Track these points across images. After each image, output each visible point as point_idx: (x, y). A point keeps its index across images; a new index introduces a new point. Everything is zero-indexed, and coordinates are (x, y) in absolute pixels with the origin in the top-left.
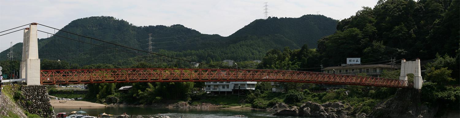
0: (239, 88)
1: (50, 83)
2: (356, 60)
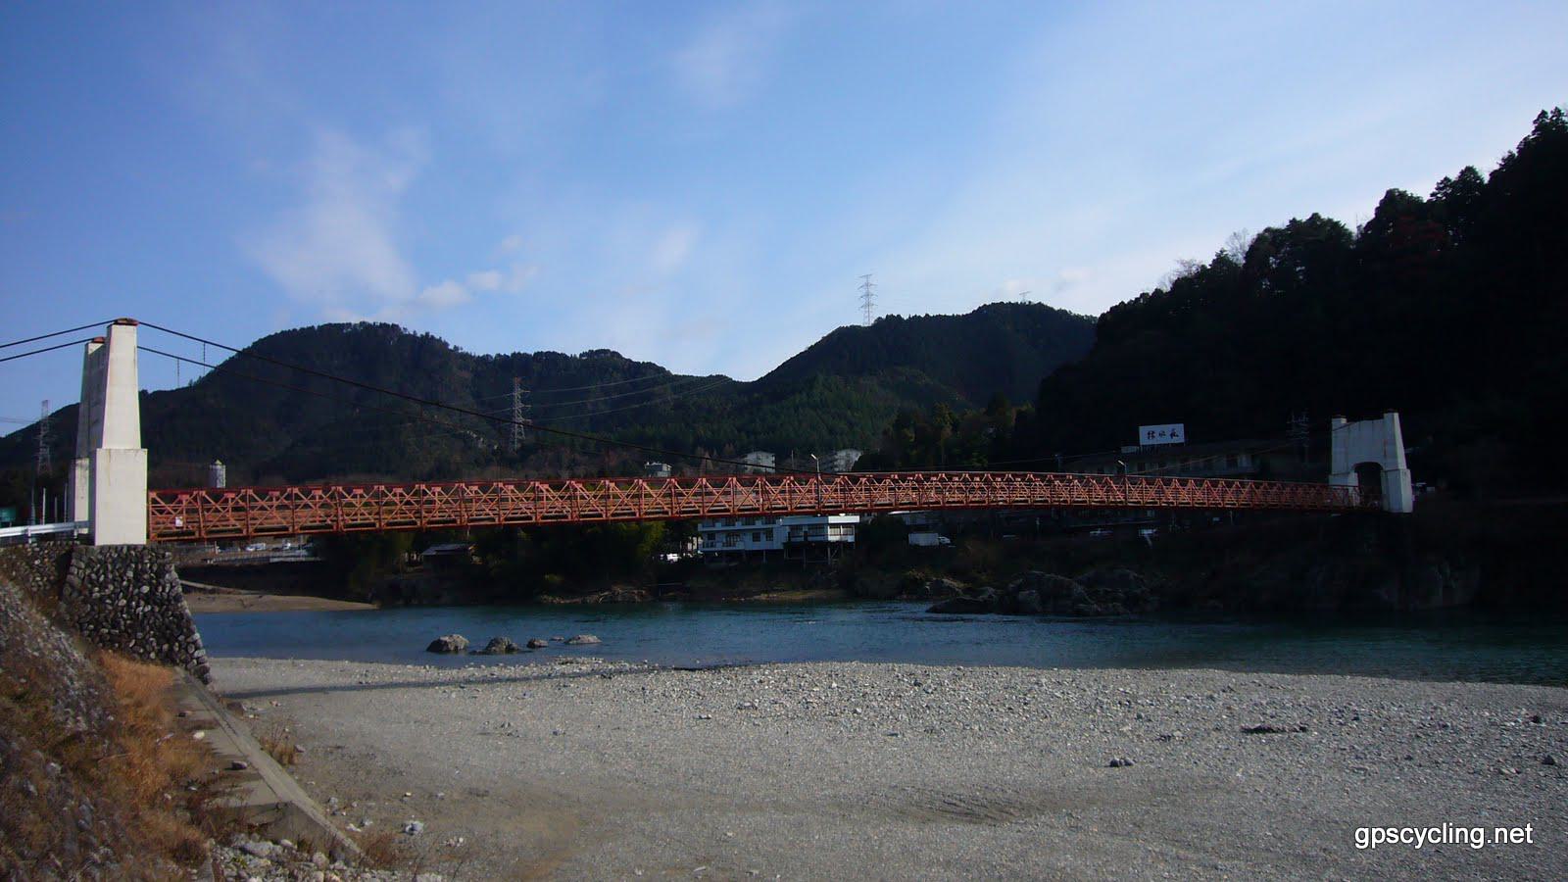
0: (806, 538)
1: (184, 538)
2: (1168, 434)
